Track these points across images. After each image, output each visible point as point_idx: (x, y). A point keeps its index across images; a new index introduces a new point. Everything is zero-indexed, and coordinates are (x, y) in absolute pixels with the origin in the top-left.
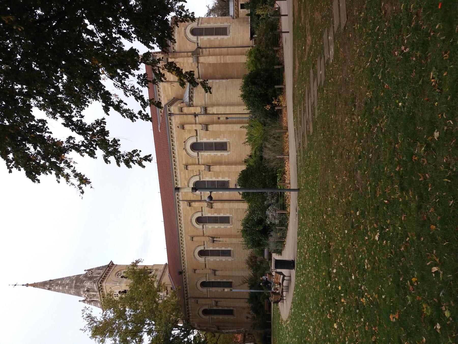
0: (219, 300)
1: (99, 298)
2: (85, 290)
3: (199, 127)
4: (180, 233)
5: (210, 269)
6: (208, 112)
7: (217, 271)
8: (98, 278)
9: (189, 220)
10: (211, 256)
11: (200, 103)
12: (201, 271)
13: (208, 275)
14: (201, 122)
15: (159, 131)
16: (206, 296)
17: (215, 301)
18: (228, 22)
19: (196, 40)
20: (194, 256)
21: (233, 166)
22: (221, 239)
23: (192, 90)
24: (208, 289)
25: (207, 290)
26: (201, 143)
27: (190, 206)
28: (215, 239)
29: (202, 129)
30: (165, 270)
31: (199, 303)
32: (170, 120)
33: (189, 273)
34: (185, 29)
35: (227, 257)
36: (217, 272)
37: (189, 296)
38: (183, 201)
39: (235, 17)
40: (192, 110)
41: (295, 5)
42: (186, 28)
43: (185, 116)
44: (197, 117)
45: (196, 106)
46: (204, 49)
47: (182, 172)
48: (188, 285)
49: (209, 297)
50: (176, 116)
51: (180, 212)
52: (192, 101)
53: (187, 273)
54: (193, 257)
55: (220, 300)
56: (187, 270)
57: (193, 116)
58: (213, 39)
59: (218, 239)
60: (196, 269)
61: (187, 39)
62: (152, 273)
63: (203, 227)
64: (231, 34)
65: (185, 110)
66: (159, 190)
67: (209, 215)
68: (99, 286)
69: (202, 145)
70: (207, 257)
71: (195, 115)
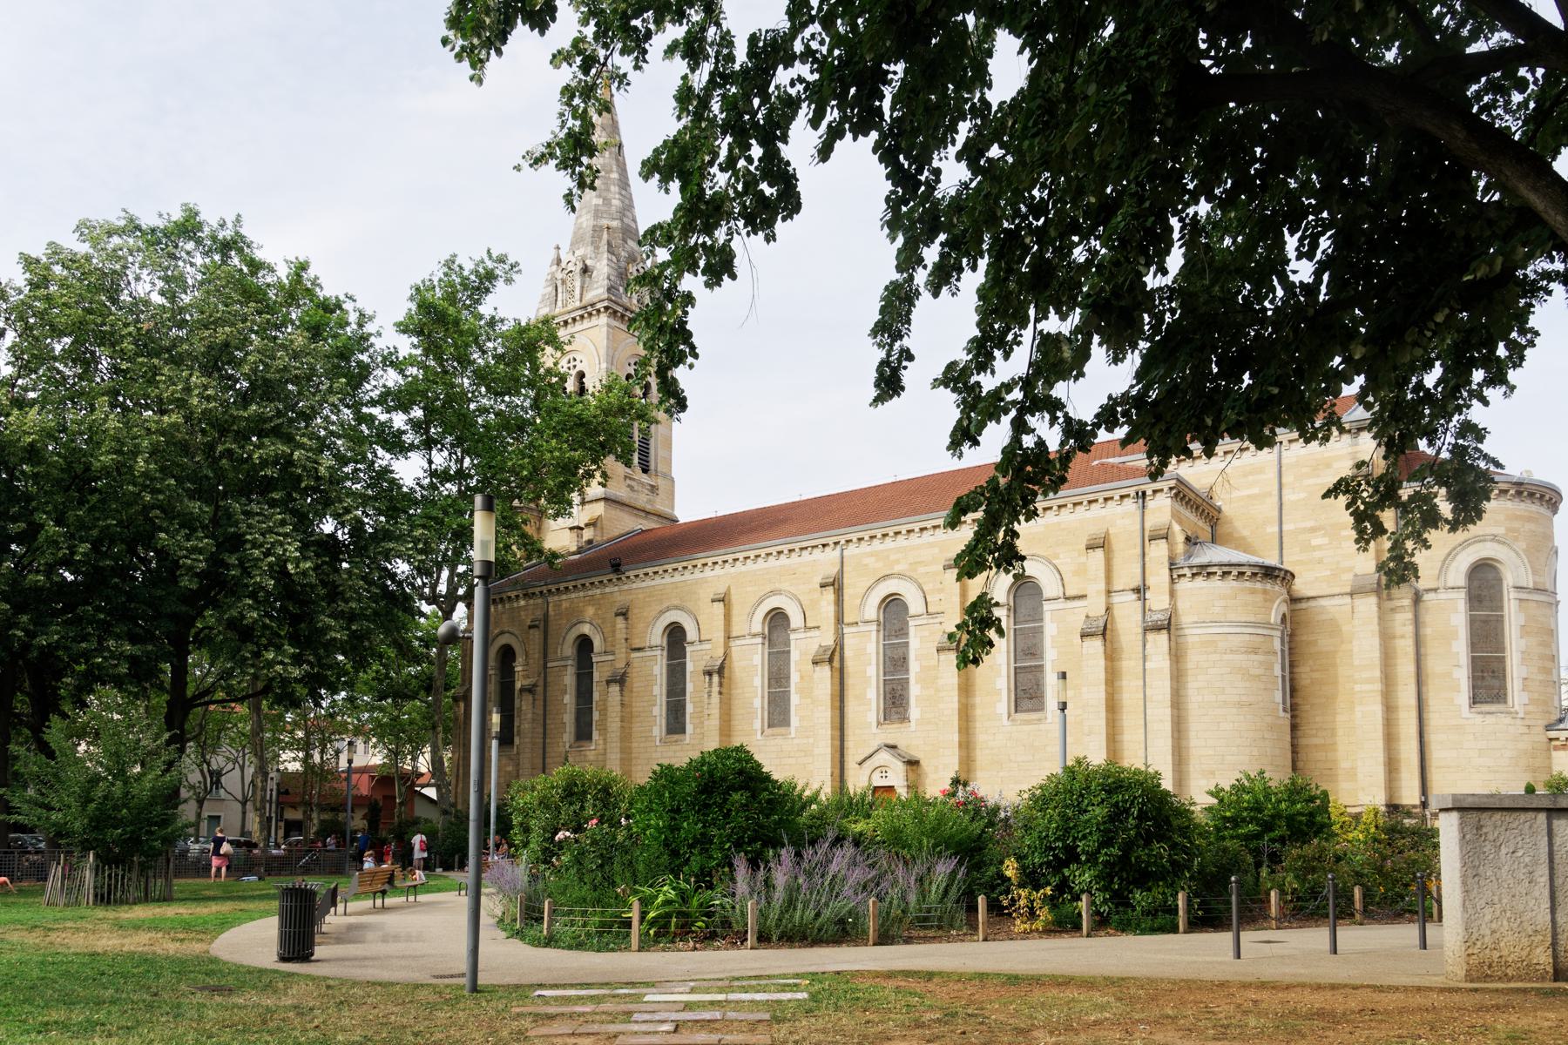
0: (540, 696)
1: (566, 309)
2: (588, 262)
3: (1095, 606)
4: (737, 555)
5: (628, 664)
6: (1151, 636)
7: (621, 690)
8: (625, 300)
9: (778, 586)
10: (668, 665)
11: (1182, 605)
12: (621, 635)
13: (610, 658)
14: (1117, 612)
15: (1096, 463)
16: (551, 656)
17: (535, 685)
18: (1531, 708)
19: (1450, 584)
20: (668, 609)
21: (956, 737)
22: (715, 698)
23: (1235, 572)
24: (570, 662)
25: (567, 658)
26: (1037, 616)
27: (823, 586)
28: (716, 678)
29: (1087, 617)
30: (655, 518)
31: (532, 631)
32: (1122, 497)
33: (618, 593)
34: (1494, 538)
35: (664, 722)
36: (618, 688)
37: (550, 599)
38: (839, 561)
39: (1553, 734)
40: (1159, 577)
41: (1037, 995)
42: (1499, 542)
43: (1138, 550)
44: (1134, 596)
45: (1172, 594)
46: (1410, 615)
47: (936, 550)
48: (581, 594)
49: (549, 665)
50: (1138, 519)
51: (805, 553)
52: (1194, 575)
53: (616, 589)
54: (665, 605)
55: (540, 703)
56: (626, 587)
57: (1137, 582)
58: (1454, 650)
59: (716, 689)
60: (626, 619)
61: (1454, 549)
62: (644, 476)
63: (755, 635)
64: (1479, 718)
65: (1159, 551)
66: (904, 476)
67: (795, 656)
68: (599, 306)
69: (1034, 621)
70: (665, 653)
71: (1140, 591)
